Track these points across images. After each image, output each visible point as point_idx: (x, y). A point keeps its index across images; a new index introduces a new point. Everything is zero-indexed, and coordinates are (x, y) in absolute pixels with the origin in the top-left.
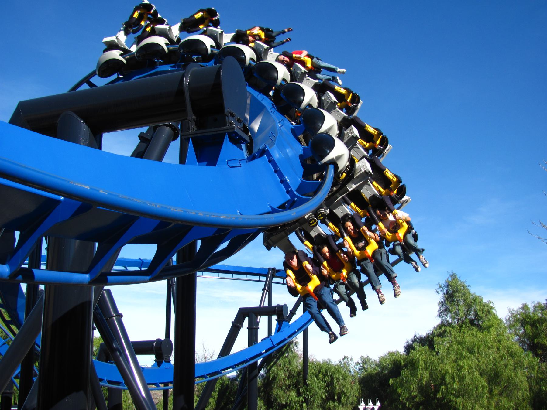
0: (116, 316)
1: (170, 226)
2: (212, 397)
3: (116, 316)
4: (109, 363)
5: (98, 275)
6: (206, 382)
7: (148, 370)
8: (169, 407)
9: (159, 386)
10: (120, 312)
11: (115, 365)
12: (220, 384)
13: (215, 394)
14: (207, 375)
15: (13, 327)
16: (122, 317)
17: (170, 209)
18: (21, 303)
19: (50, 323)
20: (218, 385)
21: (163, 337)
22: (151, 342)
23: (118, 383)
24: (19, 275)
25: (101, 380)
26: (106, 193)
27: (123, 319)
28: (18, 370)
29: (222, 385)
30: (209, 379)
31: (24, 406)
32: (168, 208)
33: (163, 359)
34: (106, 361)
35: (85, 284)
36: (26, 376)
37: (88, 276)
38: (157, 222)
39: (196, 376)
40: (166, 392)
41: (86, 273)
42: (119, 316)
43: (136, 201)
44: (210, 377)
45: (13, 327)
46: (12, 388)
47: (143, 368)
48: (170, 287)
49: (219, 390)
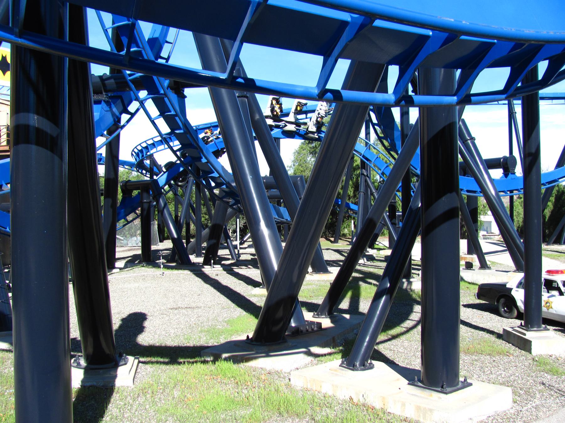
0: (471, 139)
1: (523, 47)
2: (550, 201)
3: (471, 139)
4: (467, 176)
5: (464, 96)
6: (545, 189)
7: (498, 181)
8: (515, 210)
9: (507, 193)
10: (473, 136)
11: (473, 178)
12: (557, 191)
13: (553, 199)
14: (546, 183)
15: (392, 153)
16: (475, 140)
17: (523, 31)
18: (397, 134)
19: (426, 141)
20: (555, 192)
21: (507, 155)
22: (500, 159)
23: (475, 192)
24: (402, 101)
25: (462, 190)
26: (468, 23)
27: (475, 141)
28: (400, 184)
29: (558, 191)
30: (548, 186)
31: (410, 206)
32: (522, 30)
33: (509, 171)
34: (464, 175)
35: (453, 104)
36: (406, 190)
37: (455, 98)
38: (512, 44)
39: (384, 270)
40: (511, 198)
41: (454, 95)
42: (473, 139)
43: (494, 27)
44: (548, 185)
45: (392, 153)
46: (395, 198)
47: (493, 180)
48: (511, 115)
49: (556, 195)
